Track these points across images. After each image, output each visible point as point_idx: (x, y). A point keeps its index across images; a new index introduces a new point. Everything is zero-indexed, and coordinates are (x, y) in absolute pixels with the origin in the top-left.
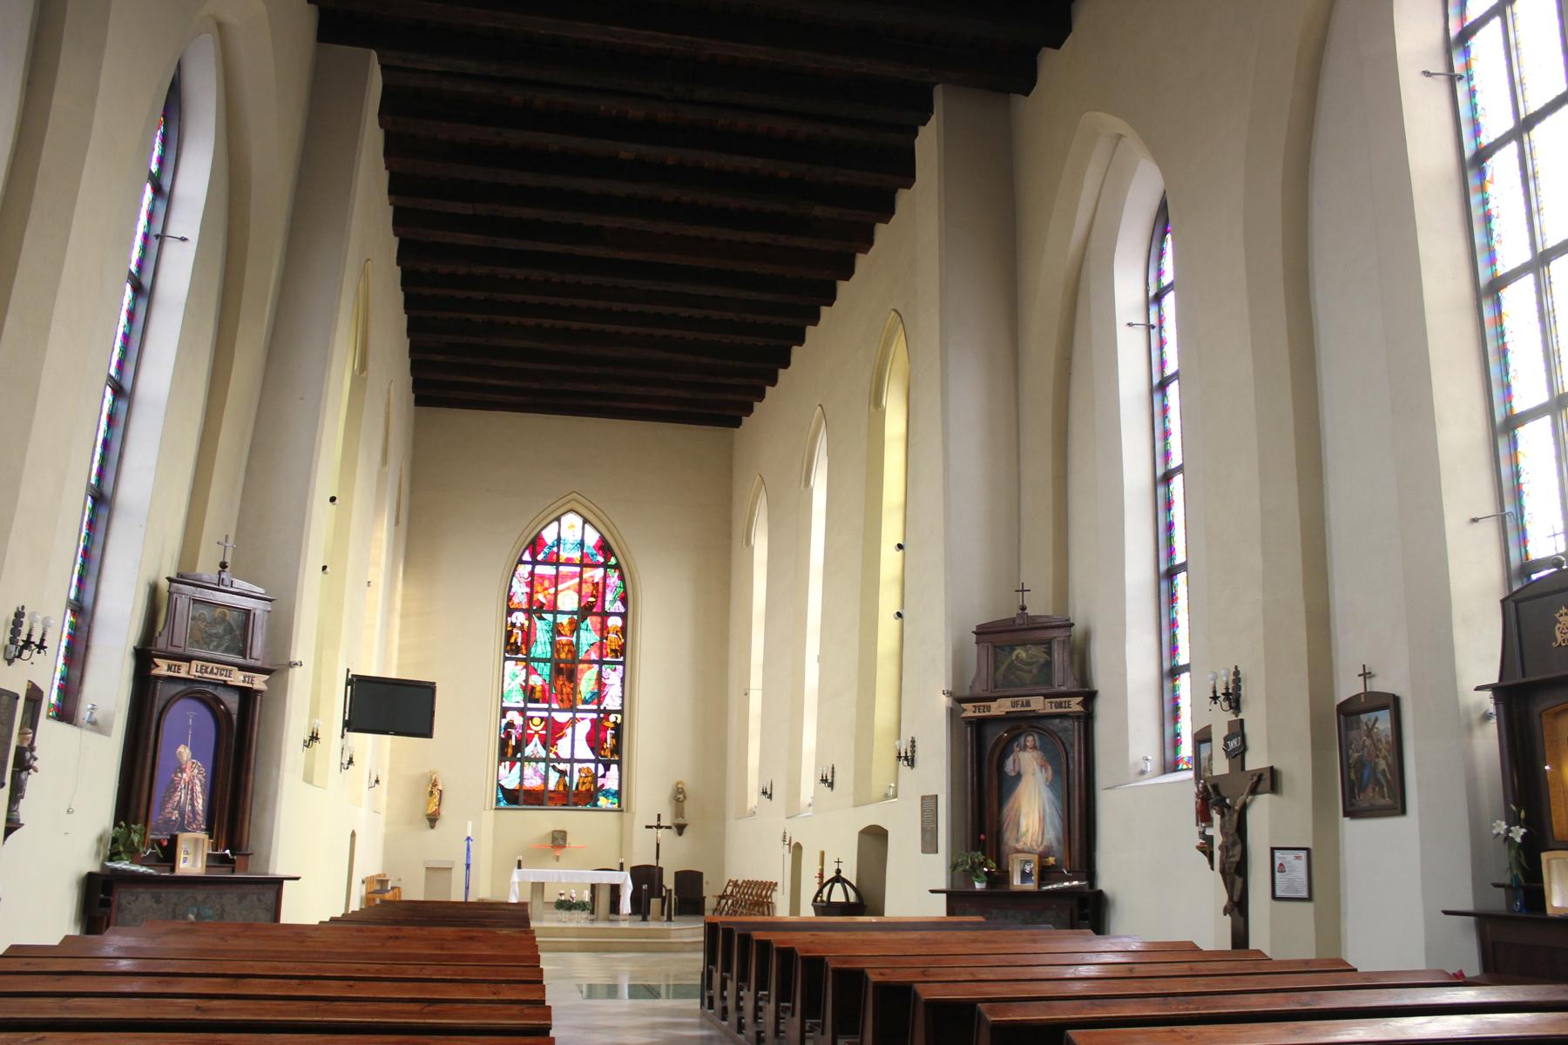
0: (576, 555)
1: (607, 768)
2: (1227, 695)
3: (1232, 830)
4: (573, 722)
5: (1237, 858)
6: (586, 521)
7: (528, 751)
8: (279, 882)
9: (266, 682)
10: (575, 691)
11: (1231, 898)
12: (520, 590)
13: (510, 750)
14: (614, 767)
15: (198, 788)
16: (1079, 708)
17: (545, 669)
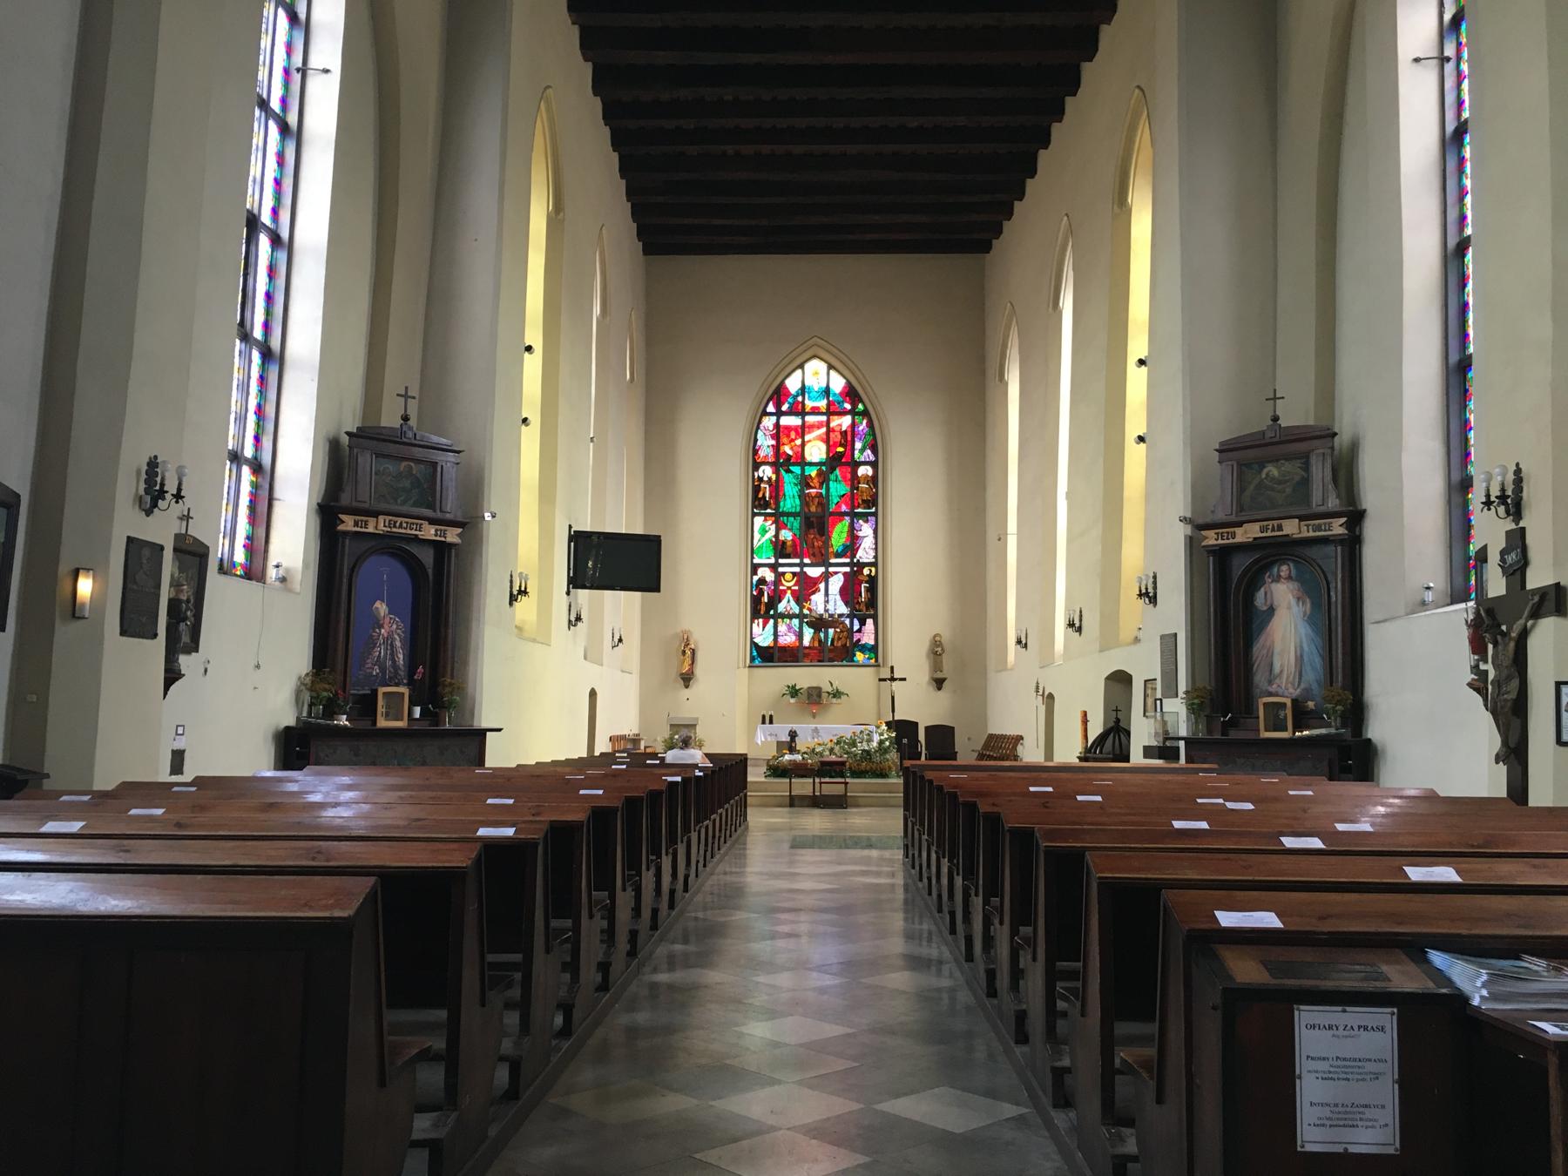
0: (822, 404)
1: (863, 623)
2: (1503, 498)
3: (1507, 661)
4: (826, 577)
5: (1513, 695)
6: (830, 367)
7: (781, 607)
8: (481, 734)
9: (459, 535)
10: (827, 543)
11: (1505, 743)
12: (765, 443)
13: (763, 606)
14: (870, 622)
15: (398, 644)
16: (1342, 531)
17: (796, 523)
